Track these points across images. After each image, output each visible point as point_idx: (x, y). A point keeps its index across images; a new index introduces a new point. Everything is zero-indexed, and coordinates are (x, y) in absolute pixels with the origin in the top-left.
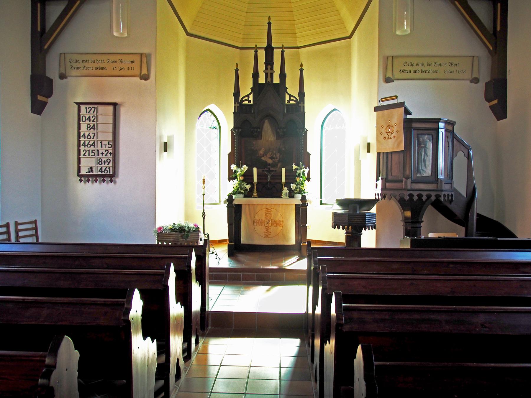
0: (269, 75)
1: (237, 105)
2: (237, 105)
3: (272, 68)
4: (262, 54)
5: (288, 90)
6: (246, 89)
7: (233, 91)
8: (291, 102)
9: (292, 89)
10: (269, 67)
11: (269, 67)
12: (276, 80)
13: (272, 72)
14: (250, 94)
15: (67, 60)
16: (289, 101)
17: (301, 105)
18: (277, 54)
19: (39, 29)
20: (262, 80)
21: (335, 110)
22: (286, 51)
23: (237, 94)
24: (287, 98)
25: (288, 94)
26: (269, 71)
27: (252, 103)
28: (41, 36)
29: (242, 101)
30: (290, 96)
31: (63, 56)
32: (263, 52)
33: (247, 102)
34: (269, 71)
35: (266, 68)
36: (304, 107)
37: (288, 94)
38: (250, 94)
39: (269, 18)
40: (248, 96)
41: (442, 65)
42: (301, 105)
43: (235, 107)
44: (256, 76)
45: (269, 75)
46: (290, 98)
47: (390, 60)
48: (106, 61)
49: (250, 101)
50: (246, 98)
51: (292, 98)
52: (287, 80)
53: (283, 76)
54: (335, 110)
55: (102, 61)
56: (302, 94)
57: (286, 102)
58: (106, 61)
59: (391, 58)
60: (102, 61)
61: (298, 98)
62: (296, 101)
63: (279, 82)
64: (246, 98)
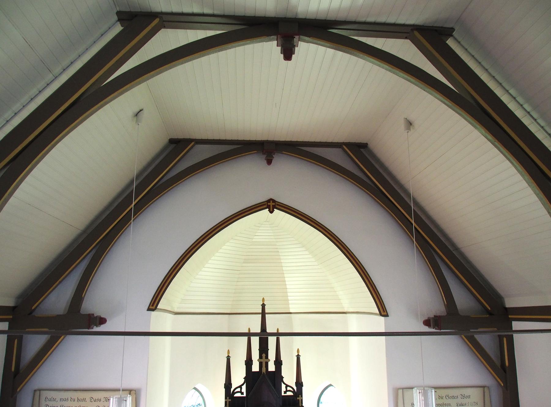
0: (263, 364)
1: (228, 400)
2: (228, 400)
3: (267, 357)
4: (255, 341)
5: (284, 380)
6: (238, 378)
7: (224, 382)
8: (289, 393)
9: (289, 377)
10: (264, 355)
11: (264, 355)
12: (272, 367)
13: (266, 360)
14: (243, 385)
15: (43, 398)
16: (285, 392)
17: (299, 398)
18: (272, 341)
19: (13, 369)
20: (255, 368)
21: (330, 385)
22: (282, 338)
23: (228, 385)
24: (283, 388)
25: (284, 383)
26: (264, 360)
27: (245, 395)
28: (15, 376)
29: (234, 393)
30: (287, 386)
31: (38, 392)
32: (257, 339)
33: (239, 395)
34: (264, 360)
35: (261, 357)
36: (302, 400)
37: (284, 383)
38: (243, 385)
39: (263, 300)
40: (240, 387)
41: (453, 397)
42: (299, 398)
43: (226, 402)
44: (249, 363)
45: (263, 364)
46: (286, 388)
47: (400, 391)
48: (88, 399)
49: (242, 393)
50: (239, 390)
51: (289, 388)
52: (283, 367)
53: (278, 363)
54: (330, 385)
55: (84, 400)
56: (299, 384)
57: (283, 394)
58: (88, 399)
59: (401, 390)
60: (84, 400)
61: (295, 388)
62: (293, 392)
63: (274, 370)
64: (239, 390)
